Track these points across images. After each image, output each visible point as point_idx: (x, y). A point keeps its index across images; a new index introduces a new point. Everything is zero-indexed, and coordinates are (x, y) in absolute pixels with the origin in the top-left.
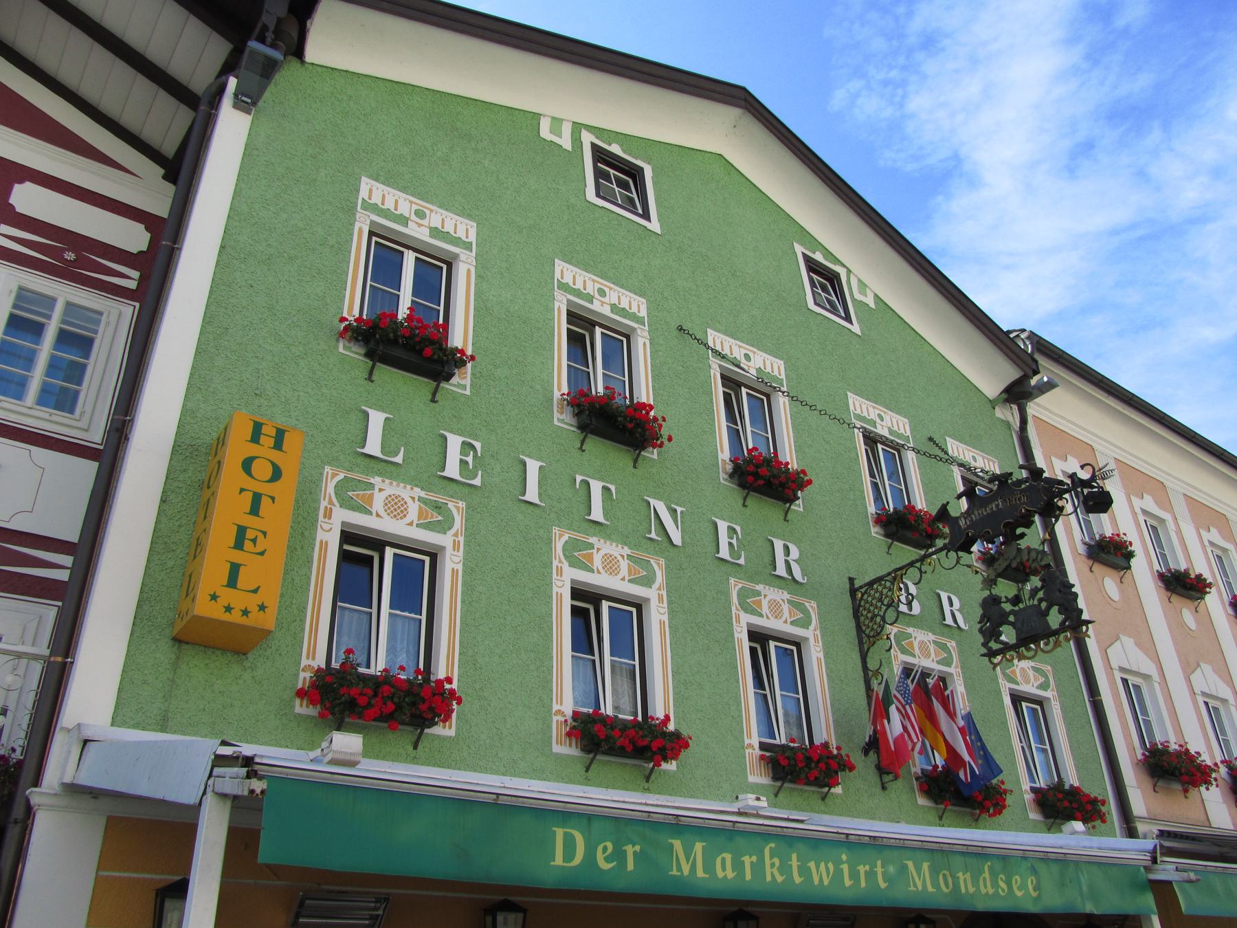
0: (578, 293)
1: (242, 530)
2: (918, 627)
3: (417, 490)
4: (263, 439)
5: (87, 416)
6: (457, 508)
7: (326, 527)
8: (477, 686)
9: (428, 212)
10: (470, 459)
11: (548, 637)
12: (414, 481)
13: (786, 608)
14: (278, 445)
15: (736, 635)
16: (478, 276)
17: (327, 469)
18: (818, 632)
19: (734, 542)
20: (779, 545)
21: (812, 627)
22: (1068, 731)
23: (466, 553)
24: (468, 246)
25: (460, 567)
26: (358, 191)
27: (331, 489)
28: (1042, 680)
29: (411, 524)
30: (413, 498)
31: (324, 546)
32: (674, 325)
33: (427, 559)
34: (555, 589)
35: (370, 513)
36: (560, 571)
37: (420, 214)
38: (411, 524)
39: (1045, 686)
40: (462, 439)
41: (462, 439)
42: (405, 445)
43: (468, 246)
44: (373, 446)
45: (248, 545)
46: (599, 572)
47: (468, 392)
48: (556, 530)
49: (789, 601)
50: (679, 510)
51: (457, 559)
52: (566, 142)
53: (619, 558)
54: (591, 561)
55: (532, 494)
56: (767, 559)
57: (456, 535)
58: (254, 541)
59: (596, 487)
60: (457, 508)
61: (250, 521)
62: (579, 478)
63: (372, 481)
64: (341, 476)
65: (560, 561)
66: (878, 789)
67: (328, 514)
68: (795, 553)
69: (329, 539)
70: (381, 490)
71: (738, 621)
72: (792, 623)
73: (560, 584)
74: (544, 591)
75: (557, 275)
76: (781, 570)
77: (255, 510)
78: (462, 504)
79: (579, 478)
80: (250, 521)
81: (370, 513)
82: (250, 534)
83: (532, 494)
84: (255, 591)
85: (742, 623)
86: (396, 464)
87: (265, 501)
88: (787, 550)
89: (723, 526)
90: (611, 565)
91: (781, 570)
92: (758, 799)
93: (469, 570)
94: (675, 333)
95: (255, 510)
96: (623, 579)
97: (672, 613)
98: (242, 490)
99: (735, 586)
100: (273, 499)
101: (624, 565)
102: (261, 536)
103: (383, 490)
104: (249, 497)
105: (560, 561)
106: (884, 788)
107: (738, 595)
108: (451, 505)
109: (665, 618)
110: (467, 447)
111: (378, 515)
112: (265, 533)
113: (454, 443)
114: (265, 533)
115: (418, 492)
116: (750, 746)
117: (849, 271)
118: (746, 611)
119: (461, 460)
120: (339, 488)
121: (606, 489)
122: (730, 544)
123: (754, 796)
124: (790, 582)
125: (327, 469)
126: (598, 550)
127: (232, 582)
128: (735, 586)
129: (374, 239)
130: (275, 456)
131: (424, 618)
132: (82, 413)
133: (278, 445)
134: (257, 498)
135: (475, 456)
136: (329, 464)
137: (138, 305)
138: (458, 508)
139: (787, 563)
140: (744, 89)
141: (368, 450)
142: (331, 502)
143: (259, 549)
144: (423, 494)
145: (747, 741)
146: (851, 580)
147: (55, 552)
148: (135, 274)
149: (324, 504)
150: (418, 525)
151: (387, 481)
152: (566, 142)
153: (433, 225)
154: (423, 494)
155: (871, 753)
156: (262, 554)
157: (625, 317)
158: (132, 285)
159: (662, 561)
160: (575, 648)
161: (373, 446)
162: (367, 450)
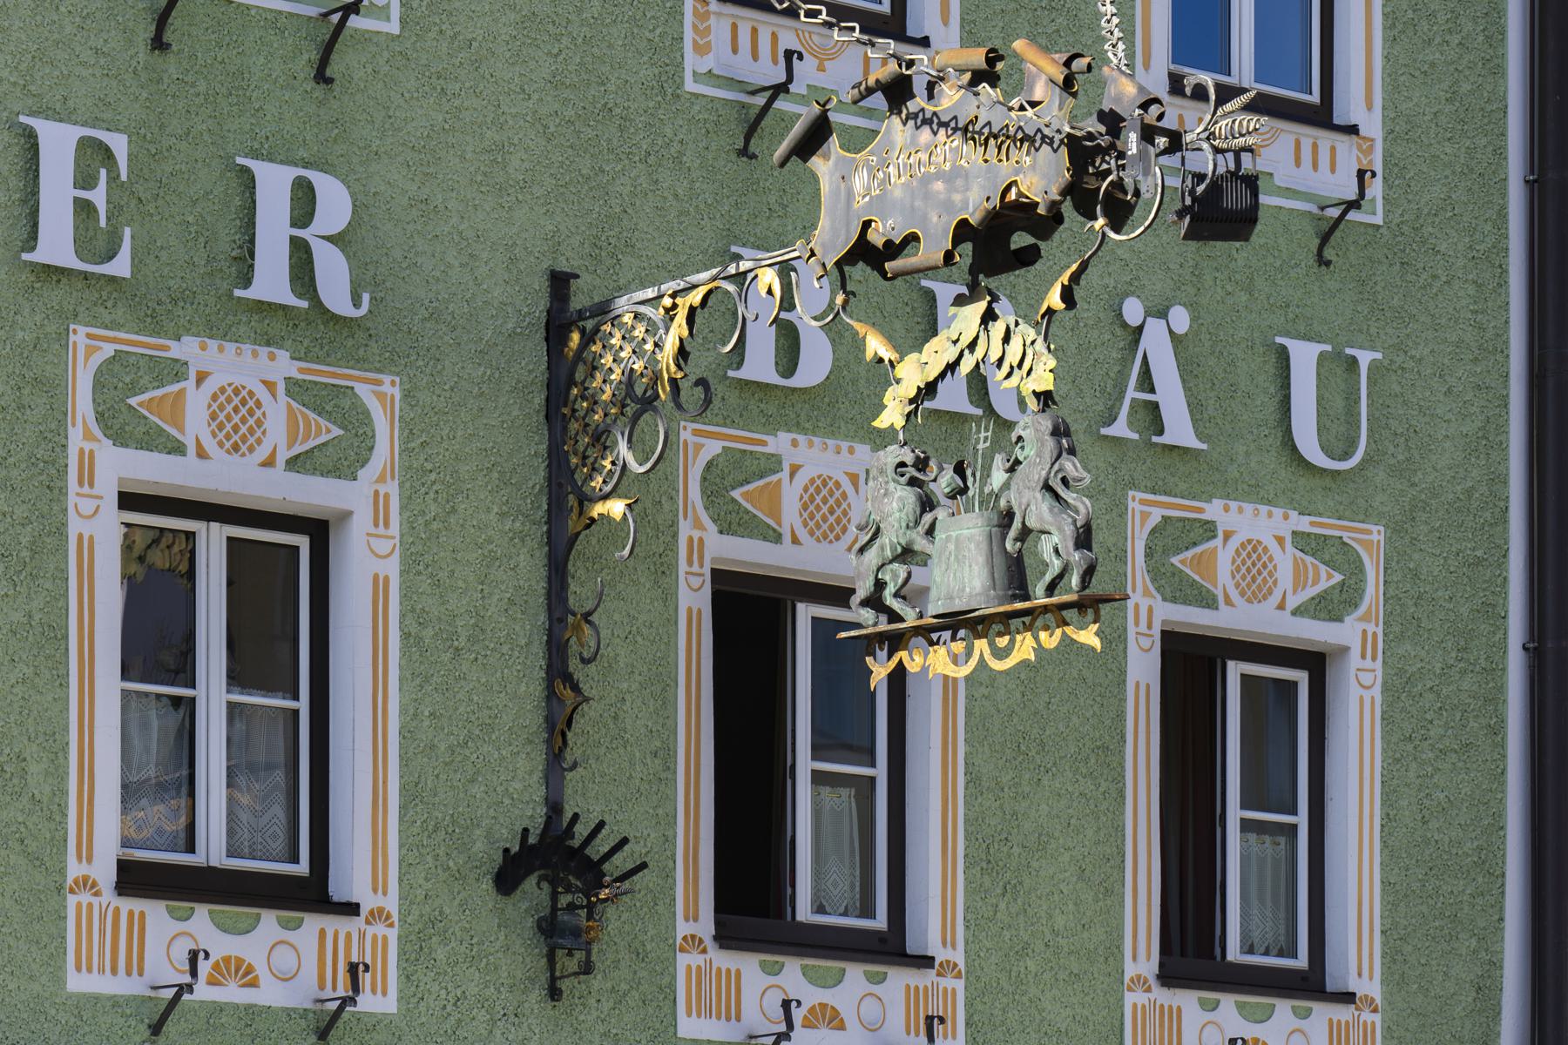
2: (798, 427)
10: (98, 196)
13: (276, 413)
15: (75, 527)
18: (392, 489)
19: (98, 196)
20: (274, 184)
22: (1394, 762)
28: (1328, 579)
31: (87, 547)
33: (303, 542)
38: (269, 463)
39: (1329, 607)
40: (77, 132)
41: (77, 132)
49: (295, 388)
54: (776, 513)
56: (226, 238)
63: (176, 350)
64: (109, 350)
66: (537, 994)
68: (335, 204)
69: (98, 532)
71: (88, 475)
72: (293, 464)
73: (87, 506)
76: (271, 281)
78: (391, 387)
85: (100, 475)
88: (304, 202)
89: (59, 143)
91: (271, 281)
96: (269, 463)
99: (87, 351)
105: (698, 525)
106: (554, 993)
107: (98, 385)
108: (362, 390)
116: (86, 884)
119: (293, 240)
122: (84, 209)
124: (305, 324)
128: (87, 351)
131: (303, 705)
135: (113, 178)
138: (381, 396)
139: (301, 254)
141: (43, 254)
145: (74, 870)
146: (560, 282)
155: (530, 883)
162: (40, 256)
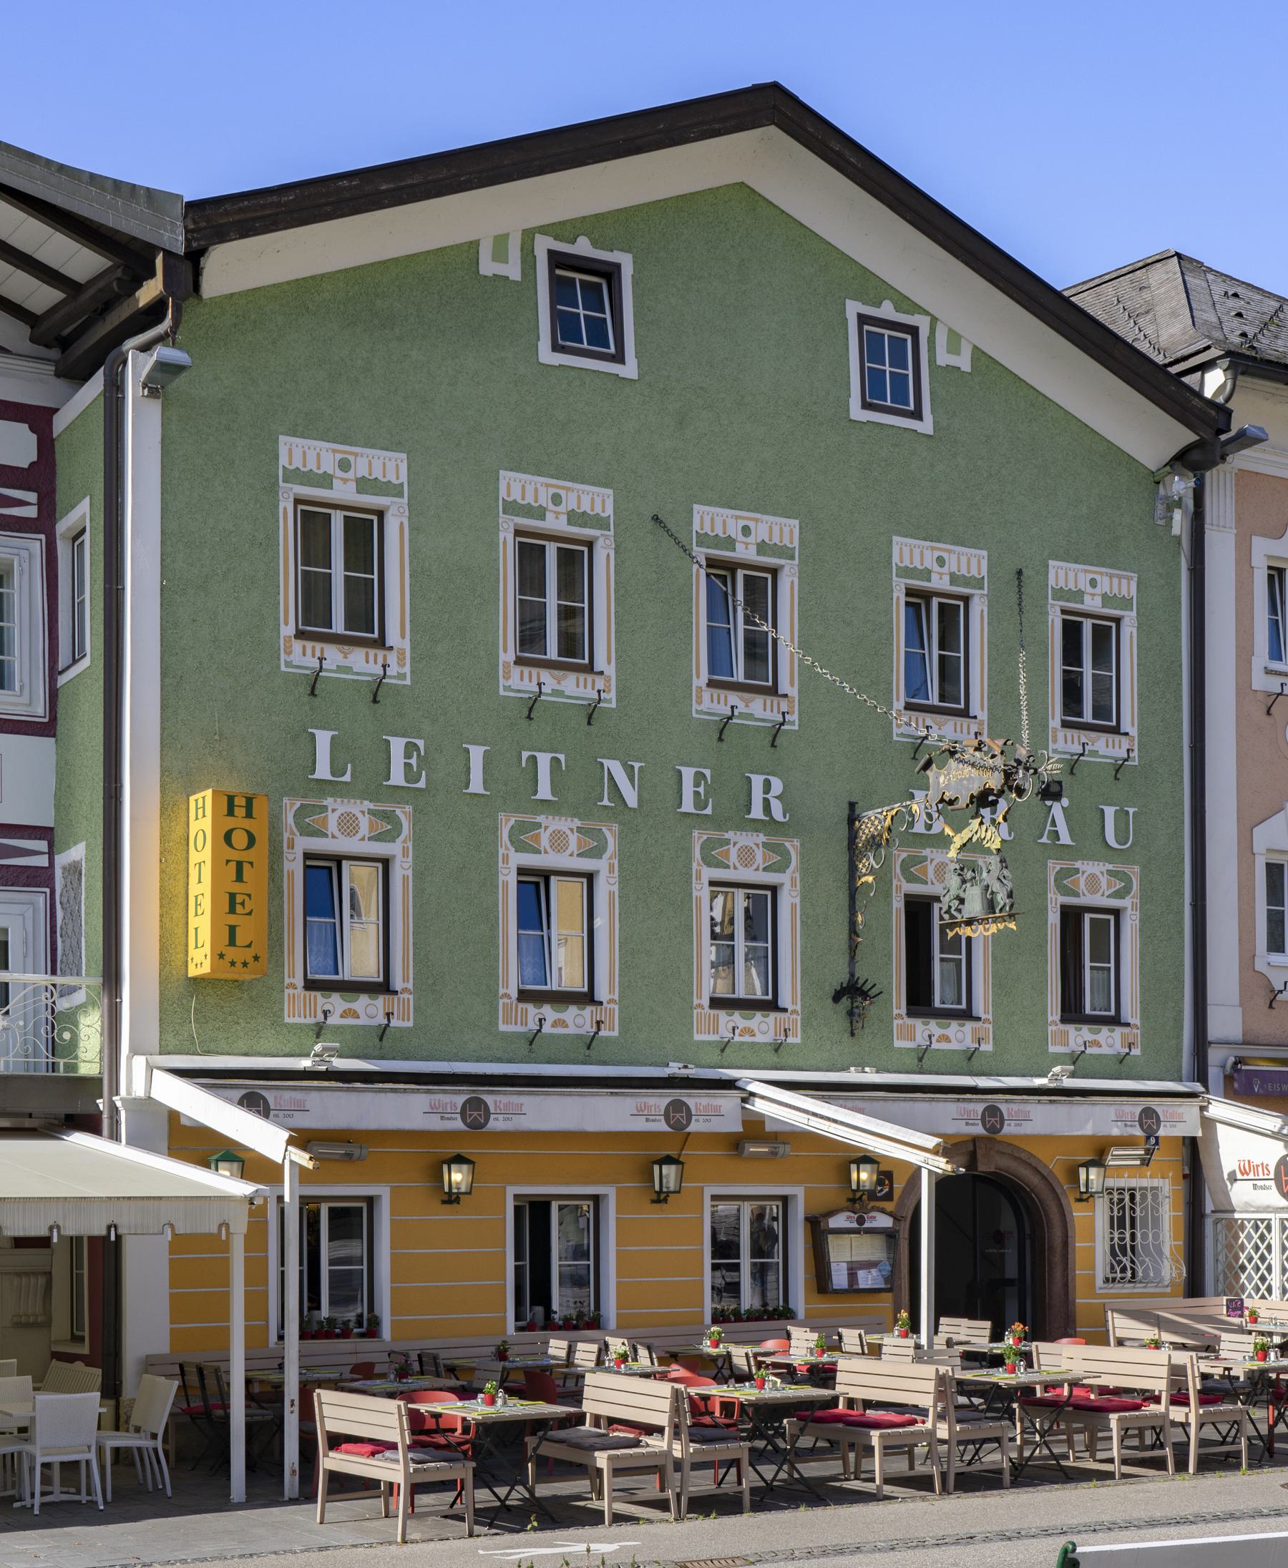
0: (527, 511)
1: (232, 896)
3: (366, 803)
4: (237, 811)
5: (26, 691)
6: (404, 814)
7: (291, 857)
8: (431, 981)
9: (351, 458)
11: (494, 927)
12: (364, 795)
14: (249, 814)
16: (412, 529)
17: (286, 800)
20: (757, 781)
21: (789, 871)
23: (415, 857)
24: (396, 491)
25: (410, 873)
26: (277, 457)
27: (290, 820)
29: (363, 839)
30: (363, 812)
32: (649, 514)
33: (375, 518)
34: (501, 878)
35: (326, 836)
36: (506, 859)
37: (344, 465)
38: (363, 839)
42: (353, 762)
43: (396, 491)
44: (323, 771)
45: (239, 909)
46: (546, 852)
47: (408, 682)
48: (501, 816)
50: (637, 765)
51: (406, 865)
52: (513, 271)
53: (568, 832)
55: (476, 785)
57: (405, 841)
58: (243, 904)
59: (544, 760)
60: (404, 814)
61: (237, 888)
62: (525, 755)
64: (298, 804)
65: (507, 849)
66: (847, 1035)
67: (291, 845)
68: (777, 786)
69: (294, 867)
70: (333, 811)
73: (505, 871)
74: (490, 883)
75: (503, 493)
76: (757, 812)
77: (239, 878)
79: (525, 755)
80: (237, 888)
81: (326, 836)
82: (239, 899)
83: (476, 785)
84: (249, 946)
86: (346, 783)
87: (246, 867)
88: (767, 787)
89: (688, 774)
90: (559, 842)
91: (757, 812)
92: (686, 1067)
93: (419, 875)
94: (650, 525)
95: (239, 878)
97: (623, 881)
98: (228, 861)
100: (251, 863)
101: (573, 839)
102: (247, 898)
103: (336, 809)
104: (233, 865)
105: (507, 849)
107: (702, 848)
109: (616, 888)
110: (410, 749)
111: (333, 837)
112: (249, 896)
113: (397, 745)
114: (249, 896)
115: (368, 805)
117: (934, 320)
118: (709, 865)
120: (297, 816)
121: (555, 761)
122: (697, 794)
123: (681, 1065)
124: (769, 825)
125: (286, 800)
126: (546, 828)
127: (232, 942)
129: (300, 507)
130: (247, 824)
132: (22, 688)
133: (249, 814)
134: (239, 865)
135: (419, 755)
136: (288, 795)
137: (42, 537)
140: (775, 86)
142: (292, 833)
143: (247, 911)
144: (371, 806)
145: (696, 1002)
147: (22, 838)
148: (32, 497)
149: (286, 835)
150: (370, 839)
151: (339, 800)
152: (513, 271)
153: (359, 475)
154: (371, 806)
156: (250, 914)
157: (584, 525)
158: (31, 512)
159: (616, 827)
160: (522, 924)
161: (323, 771)
